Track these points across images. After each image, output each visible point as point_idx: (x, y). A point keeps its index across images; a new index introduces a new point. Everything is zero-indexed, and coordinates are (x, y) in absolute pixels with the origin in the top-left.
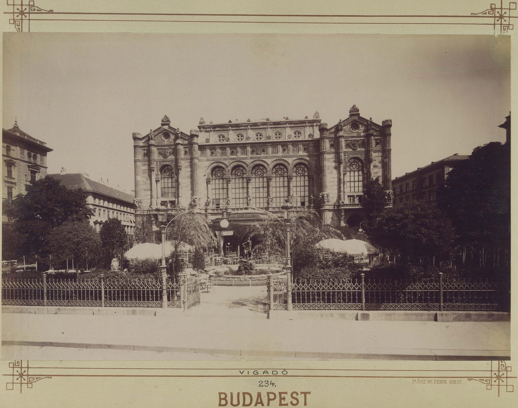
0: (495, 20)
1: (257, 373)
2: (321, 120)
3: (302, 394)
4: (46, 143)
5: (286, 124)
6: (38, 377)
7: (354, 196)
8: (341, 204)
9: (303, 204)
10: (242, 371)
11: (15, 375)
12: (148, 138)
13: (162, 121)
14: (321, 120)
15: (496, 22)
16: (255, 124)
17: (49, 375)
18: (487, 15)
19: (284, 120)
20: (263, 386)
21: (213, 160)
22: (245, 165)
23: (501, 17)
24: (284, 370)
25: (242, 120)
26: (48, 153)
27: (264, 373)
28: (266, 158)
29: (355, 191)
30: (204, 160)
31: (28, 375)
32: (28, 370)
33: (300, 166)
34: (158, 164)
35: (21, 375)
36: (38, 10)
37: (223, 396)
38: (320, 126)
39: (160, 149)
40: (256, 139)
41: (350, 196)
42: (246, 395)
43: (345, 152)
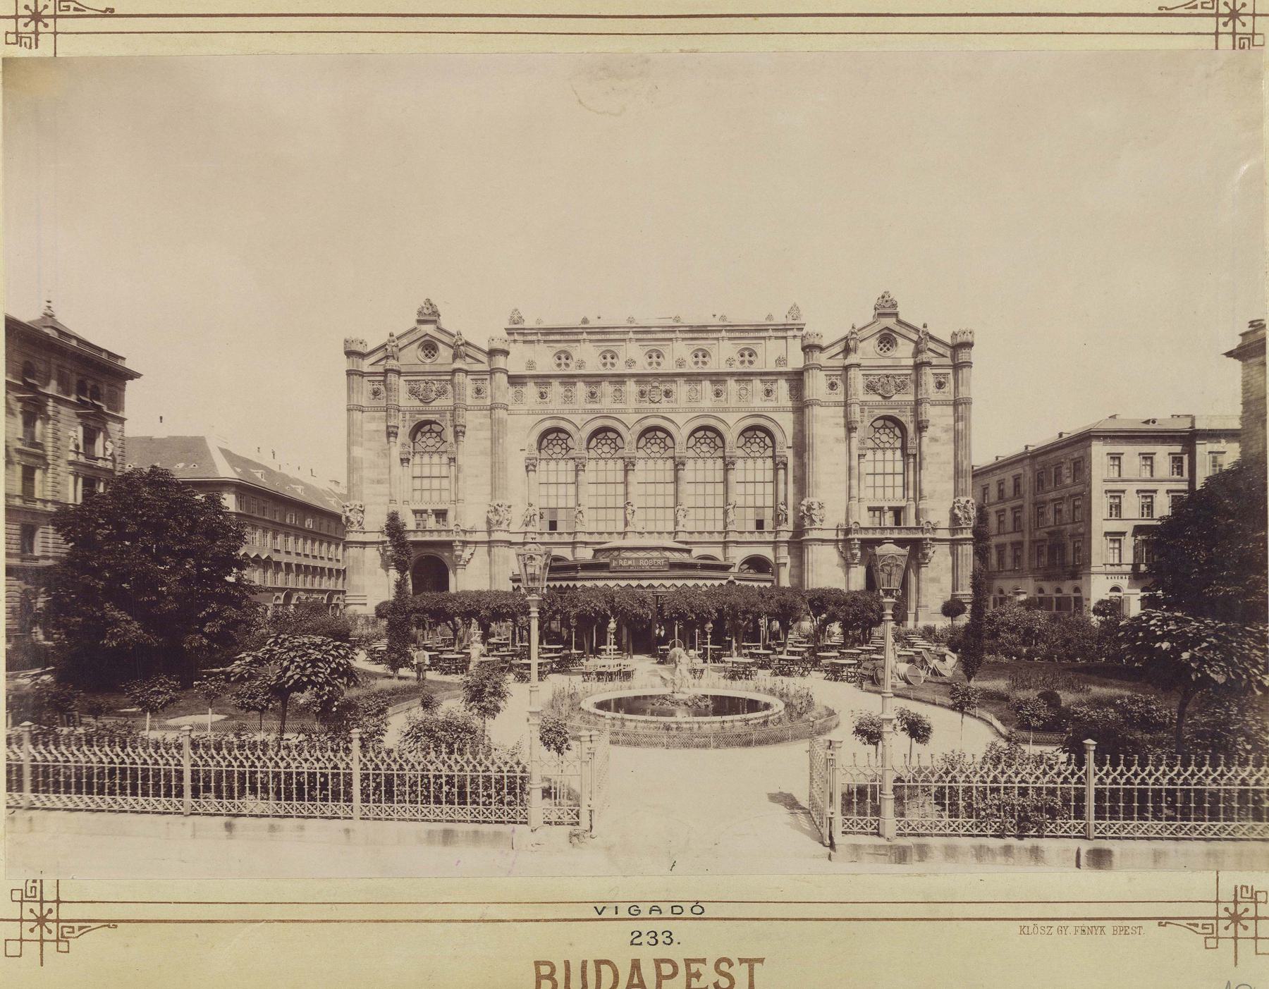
0: (1217, 22)
1: (637, 912)
2: (804, 325)
3: (743, 964)
4: (124, 359)
5: (720, 331)
6: (84, 924)
7: (883, 508)
8: (853, 527)
9: (760, 524)
10: (600, 907)
11: (26, 921)
12: (386, 351)
13: (420, 313)
14: (804, 325)
15: (1221, 29)
16: (647, 330)
17: (112, 921)
18: (1199, 11)
19: (716, 322)
20: (641, 944)
21: (543, 412)
22: (620, 428)
23: (41, 921)
24: (695, 904)
25: (615, 317)
26: (129, 382)
27: (651, 911)
28: (673, 411)
29: (886, 497)
30: (521, 412)
31: (58, 921)
32: (58, 907)
33: (755, 434)
34: (408, 416)
35: (41, 921)
36: (1197, 925)
37: (545, 970)
38: (803, 338)
39: (412, 381)
40: (647, 366)
41: (874, 507)
42: (604, 968)
43: (863, 404)
